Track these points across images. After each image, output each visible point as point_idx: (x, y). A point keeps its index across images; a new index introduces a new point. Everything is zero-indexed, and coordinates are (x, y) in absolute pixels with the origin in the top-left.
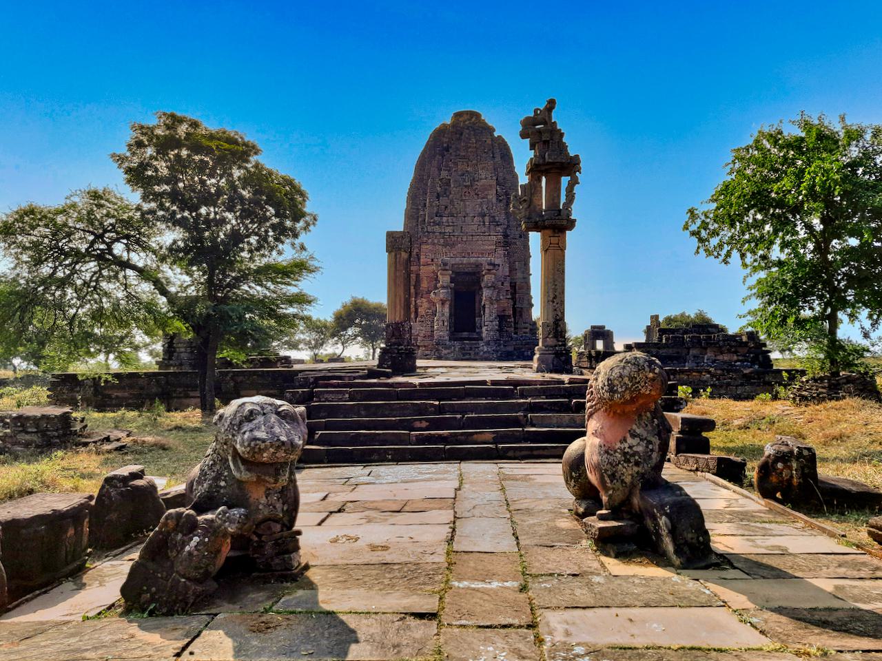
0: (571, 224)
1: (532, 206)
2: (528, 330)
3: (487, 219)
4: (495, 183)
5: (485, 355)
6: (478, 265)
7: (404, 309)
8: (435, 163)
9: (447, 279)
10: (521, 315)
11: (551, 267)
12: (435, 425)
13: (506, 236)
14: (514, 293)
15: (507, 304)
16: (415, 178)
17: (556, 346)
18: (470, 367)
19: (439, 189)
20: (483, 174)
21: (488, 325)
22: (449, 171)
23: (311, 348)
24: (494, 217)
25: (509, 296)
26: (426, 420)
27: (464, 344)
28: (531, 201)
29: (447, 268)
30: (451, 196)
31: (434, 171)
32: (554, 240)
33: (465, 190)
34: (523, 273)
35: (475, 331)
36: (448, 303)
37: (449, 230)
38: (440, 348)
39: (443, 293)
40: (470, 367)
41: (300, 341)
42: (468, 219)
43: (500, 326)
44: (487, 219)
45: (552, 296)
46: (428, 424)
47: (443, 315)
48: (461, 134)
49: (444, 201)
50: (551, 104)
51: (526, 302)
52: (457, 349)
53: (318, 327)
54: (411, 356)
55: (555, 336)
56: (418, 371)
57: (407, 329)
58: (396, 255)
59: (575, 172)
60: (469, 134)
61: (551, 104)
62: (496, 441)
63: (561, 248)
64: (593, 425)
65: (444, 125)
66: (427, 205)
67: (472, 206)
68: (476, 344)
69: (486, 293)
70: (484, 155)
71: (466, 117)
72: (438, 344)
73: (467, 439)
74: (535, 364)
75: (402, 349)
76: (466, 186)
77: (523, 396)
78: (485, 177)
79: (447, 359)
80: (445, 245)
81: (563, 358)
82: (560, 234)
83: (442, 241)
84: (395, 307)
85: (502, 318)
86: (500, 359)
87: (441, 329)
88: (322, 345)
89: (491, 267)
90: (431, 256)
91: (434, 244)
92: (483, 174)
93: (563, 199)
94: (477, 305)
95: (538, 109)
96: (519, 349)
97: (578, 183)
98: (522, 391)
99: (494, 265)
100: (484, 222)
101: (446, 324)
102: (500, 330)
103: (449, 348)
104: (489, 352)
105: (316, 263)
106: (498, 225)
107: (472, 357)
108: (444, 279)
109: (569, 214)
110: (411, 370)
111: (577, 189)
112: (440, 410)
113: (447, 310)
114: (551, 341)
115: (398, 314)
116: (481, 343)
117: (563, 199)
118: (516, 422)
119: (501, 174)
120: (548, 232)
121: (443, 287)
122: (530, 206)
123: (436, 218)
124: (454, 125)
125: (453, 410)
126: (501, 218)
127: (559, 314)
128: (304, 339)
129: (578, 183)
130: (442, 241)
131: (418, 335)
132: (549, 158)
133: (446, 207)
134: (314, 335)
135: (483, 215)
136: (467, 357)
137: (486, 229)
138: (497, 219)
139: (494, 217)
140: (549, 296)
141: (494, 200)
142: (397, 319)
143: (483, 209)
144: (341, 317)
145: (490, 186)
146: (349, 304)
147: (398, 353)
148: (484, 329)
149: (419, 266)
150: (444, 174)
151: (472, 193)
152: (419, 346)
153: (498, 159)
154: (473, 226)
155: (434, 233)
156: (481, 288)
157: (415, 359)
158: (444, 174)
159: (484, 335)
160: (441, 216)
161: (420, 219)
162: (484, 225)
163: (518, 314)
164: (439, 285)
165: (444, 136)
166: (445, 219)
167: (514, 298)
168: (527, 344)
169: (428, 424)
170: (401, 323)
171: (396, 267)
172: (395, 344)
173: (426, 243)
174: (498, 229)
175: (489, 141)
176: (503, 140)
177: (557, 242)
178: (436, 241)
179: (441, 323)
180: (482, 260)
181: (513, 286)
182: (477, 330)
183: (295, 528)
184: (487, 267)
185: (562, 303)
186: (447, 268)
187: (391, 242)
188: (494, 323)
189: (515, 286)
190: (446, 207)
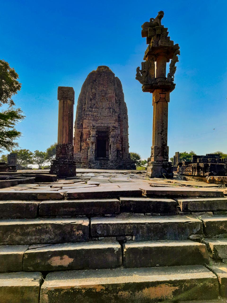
1: (148, 76)
2: (127, 157)
3: (111, 110)
4: (115, 95)
5: (111, 167)
6: (108, 128)
7: (68, 136)
8: (90, 86)
9: (95, 133)
10: (125, 151)
13: (119, 117)
14: (122, 142)
16: (81, 92)
17: (163, 161)
18: (106, 172)
19: (91, 97)
20: (110, 91)
21: (111, 155)
22: (96, 89)
23: (39, 163)
24: (114, 109)
26: (69, 253)
27: (101, 162)
28: (148, 72)
29: (95, 128)
30: (96, 100)
31: (89, 89)
32: (162, 96)
33: (102, 97)
34: (126, 133)
35: (106, 157)
36: (95, 143)
37: (95, 114)
38: (91, 164)
39: (92, 139)
40: (106, 172)
41: (34, 160)
42: (104, 110)
43: (117, 154)
44: (111, 110)
45: (160, 130)
46: (71, 260)
47: (92, 149)
48: (101, 75)
49: (93, 102)
50: (161, 15)
52: (98, 164)
53: (41, 155)
54: (73, 165)
56: (77, 175)
57: (70, 149)
58: (64, 102)
59: (176, 54)
61: (161, 15)
63: (166, 100)
65: (94, 71)
66: (86, 103)
67: (106, 104)
68: (107, 162)
69: (111, 140)
72: (90, 162)
75: (66, 161)
76: (102, 96)
78: (111, 93)
79: (94, 168)
81: (167, 169)
82: (166, 92)
83: (92, 118)
84: (63, 135)
85: (118, 151)
86: (117, 169)
87: (91, 154)
88: (43, 162)
89: (114, 128)
91: (89, 120)
92: (110, 91)
93: (168, 71)
95: (153, 19)
96: (125, 164)
97: (178, 61)
98: (186, 205)
99: (115, 127)
100: (110, 111)
101: (93, 153)
102: (117, 156)
104: (113, 166)
105: (22, 114)
106: (116, 113)
107: (105, 168)
108: (93, 133)
111: (176, 65)
113: (94, 147)
115: (64, 139)
116: (109, 162)
117: (168, 71)
119: (117, 92)
121: (93, 137)
122: (147, 76)
123: (90, 109)
124: (98, 71)
125: (108, 234)
127: (165, 141)
128: (36, 160)
129: (178, 61)
130: (92, 118)
131: (81, 158)
132: (161, 43)
133: (94, 105)
134: (39, 158)
136: (103, 167)
137: (111, 114)
138: (116, 110)
140: (158, 130)
141: (114, 102)
142: (64, 143)
143: (109, 106)
144: (50, 151)
146: (53, 145)
147: (64, 164)
148: (110, 156)
149: (82, 129)
150: (93, 90)
151: (105, 99)
152: (81, 163)
153: (116, 86)
154: (106, 112)
155: (89, 115)
156: (109, 138)
157: (75, 168)
158: (93, 90)
159: (110, 158)
160: (92, 108)
161: (83, 109)
162: (110, 112)
163: (123, 150)
164: (91, 136)
165: (94, 76)
166: (94, 109)
168: (128, 162)
169: (71, 260)
170: (67, 145)
171: (64, 109)
172: (62, 158)
173: (85, 119)
174: (116, 114)
175: (113, 78)
176: (118, 79)
177: (164, 97)
178: (90, 118)
179: (91, 153)
181: (122, 139)
182: (107, 156)
183: (175, 66)
184: (112, 128)
185: (166, 135)
186: (95, 128)
187: (61, 93)
188: (115, 153)
189: (122, 139)
190: (94, 105)
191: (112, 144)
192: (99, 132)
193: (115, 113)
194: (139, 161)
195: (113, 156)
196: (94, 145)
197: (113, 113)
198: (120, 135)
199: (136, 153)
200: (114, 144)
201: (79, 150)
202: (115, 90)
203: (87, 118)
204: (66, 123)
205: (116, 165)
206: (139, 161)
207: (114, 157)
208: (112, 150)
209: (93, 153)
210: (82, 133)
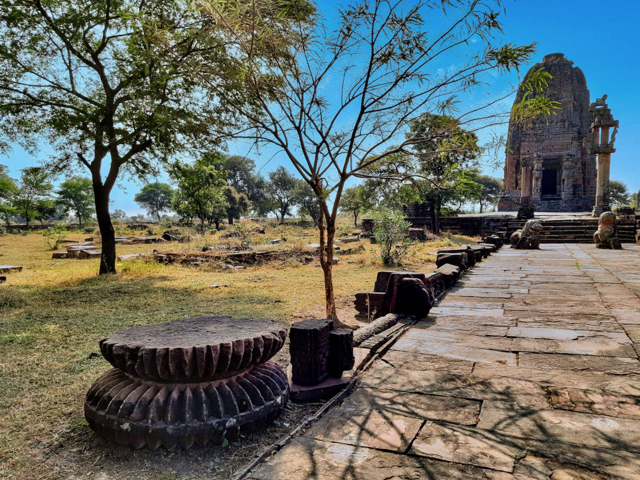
0: (613, 151)
9: (541, 165)
10: (589, 182)
11: (602, 170)
12: (552, 233)
13: (579, 133)
15: (578, 175)
21: (565, 191)
24: (571, 122)
25: (581, 171)
35: (556, 194)
44: (566, 123)
45: (602, 184)
47: (537, 186)
50: (605, 96)
51: (592, 174)
55: (604, 202)
60: (555, 70)
61: (605, 96)
62: (575, 238)
64: (599, 226)
69: (565, 173)
70: (566, 82)
71: (553, 58)
73: (565, 237)
74: (593, 214)
77: (585, 225)
80: (537, 141)
85: (575, 187)
89: (569, 157)
90: (527, 149)
91: (529, 141)
92: (564, 94)
93: (610, 140)
94: (557, 178)
99: (571, 156)
102: (574, 194)
103: (541, 205)
109: (612, 145)
110: (532, 217)
111: (616, 135)
112: (554, 229)
113: (539, 183)
114: (601, 204)
116: (561, 202)
117: (610, 140)
118: (582, 233)
119: (577, 93)
120: (602, 155)
126: (577, 121)
130: (535, 139)
135: (563, 121)
138: (574, 122)
139: (571, 122)
141: (572, 110)
145: (570, 101)
148: (563, 193)
153: (575, 81)
159: (563, 197)
163: (586, 182)
167: (584, 173)
173: (524, 141)
174: (575, 129)
176: (579, 70)
178: (531, 139)
180: (564, 153)
181: (584, 164)
182: (558, 193)
191: (566, 178)
192: (546, 161)
193: (572, 127)
194: (625, 196)
195: (568, 194)
196: (540, 181)
197: (570, 128)
198: (580, 161)
199: (616, 180)
200: (569, 178)
201: (514, 185)
202: (573, 90)
203: (527, 140)
204: (529, 183)
205: (572, 206)
206: (623, 195)
207: (569, 196)
208: (565, 186)
209: (539, 191)
210: (518, 161)
